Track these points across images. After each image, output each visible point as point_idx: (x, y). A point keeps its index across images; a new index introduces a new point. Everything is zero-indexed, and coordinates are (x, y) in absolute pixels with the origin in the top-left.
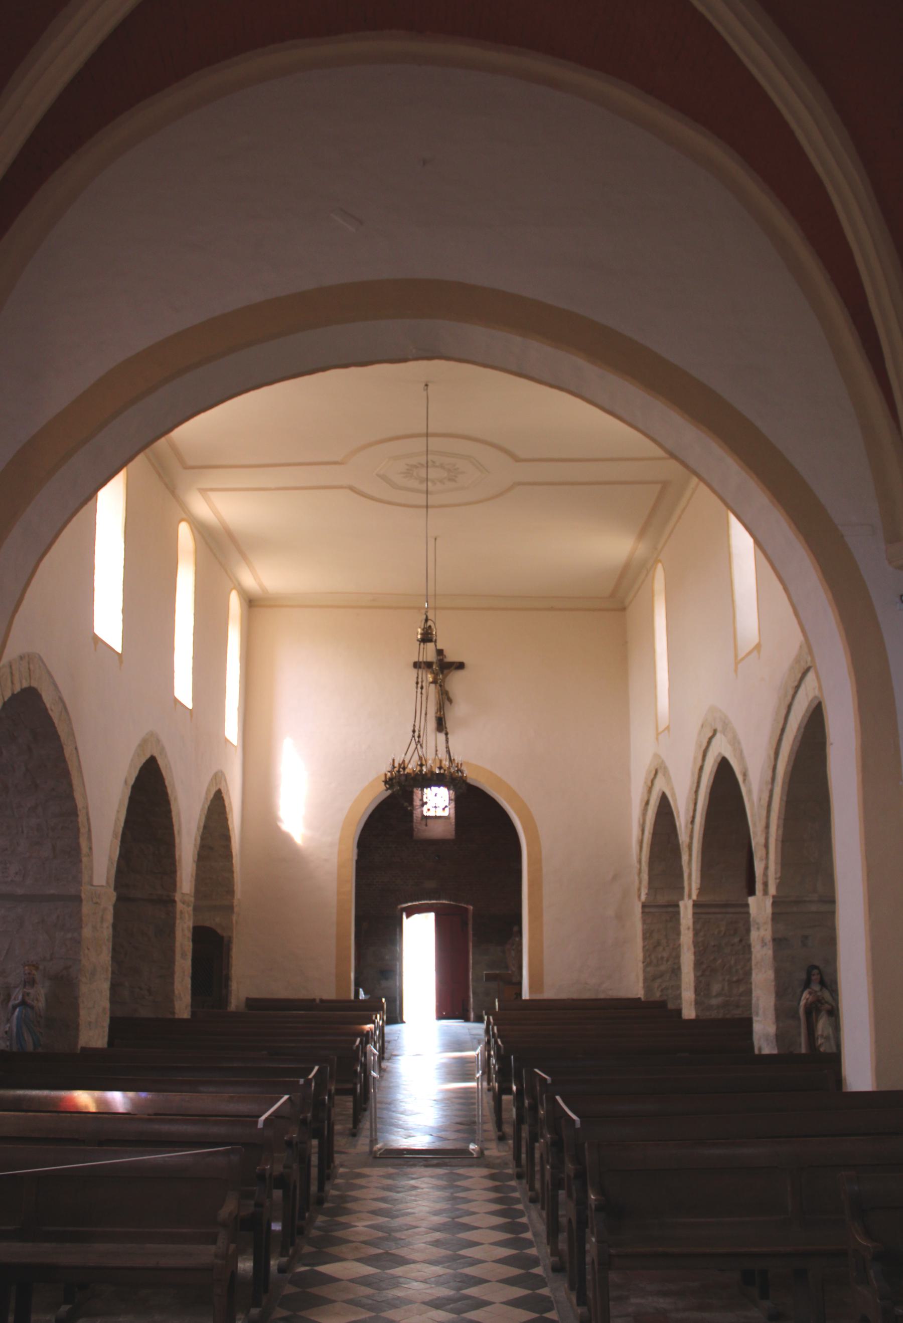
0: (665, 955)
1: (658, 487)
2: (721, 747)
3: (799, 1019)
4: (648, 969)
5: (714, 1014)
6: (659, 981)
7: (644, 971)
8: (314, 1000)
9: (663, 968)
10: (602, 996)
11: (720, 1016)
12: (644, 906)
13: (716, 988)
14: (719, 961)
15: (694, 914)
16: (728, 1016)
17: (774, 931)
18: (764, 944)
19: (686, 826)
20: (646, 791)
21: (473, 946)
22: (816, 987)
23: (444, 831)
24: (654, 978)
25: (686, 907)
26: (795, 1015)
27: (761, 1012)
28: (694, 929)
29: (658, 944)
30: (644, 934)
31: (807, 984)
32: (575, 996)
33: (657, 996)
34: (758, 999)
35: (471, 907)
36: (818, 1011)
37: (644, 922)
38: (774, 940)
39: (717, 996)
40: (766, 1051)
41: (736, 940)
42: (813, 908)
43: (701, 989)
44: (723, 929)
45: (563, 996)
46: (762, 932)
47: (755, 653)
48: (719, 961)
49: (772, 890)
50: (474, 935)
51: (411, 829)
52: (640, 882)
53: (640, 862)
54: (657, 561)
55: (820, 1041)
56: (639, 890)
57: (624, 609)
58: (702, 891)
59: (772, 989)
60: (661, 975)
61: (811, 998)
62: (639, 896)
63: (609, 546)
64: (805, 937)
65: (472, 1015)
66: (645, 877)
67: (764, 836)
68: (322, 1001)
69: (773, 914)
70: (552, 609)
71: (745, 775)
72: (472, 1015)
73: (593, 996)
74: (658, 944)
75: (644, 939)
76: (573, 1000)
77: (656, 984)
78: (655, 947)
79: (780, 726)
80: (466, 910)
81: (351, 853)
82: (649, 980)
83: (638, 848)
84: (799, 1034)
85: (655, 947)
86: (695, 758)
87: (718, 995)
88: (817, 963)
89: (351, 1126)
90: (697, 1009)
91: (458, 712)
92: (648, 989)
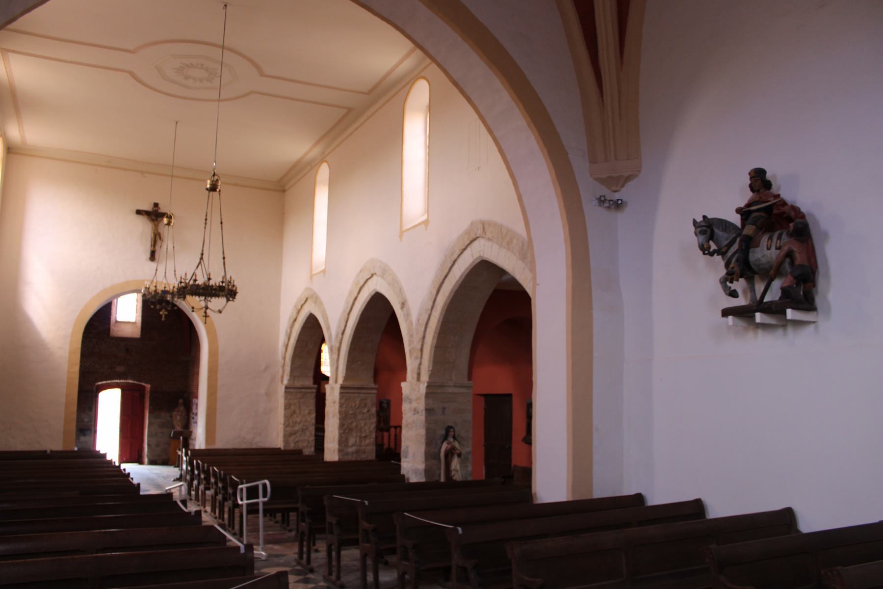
0: (298, 420)
1: (345, 111)
2: (378, 285)
3: (440, 460)
4: (288, 429)
5: (349, 458)
6: (294, 436)
7: (285, 430)
8: (45, 451)
9: (296, 428)
10: (254, 447)
11: (354, 459)
12: (286, 388)
13: (352, 441)
14: (354, 424)
15: (341, 393)
16: (359, 459)
17: (427, 404)
18: (416, 411)
19: (337, 336)
20: (295, 312)
21: (150, 413)
22: (451, 439)
23: (135, 332)
24: (291, 435)
25: (332, 389)
26: (437, 457)
27: (410, 456)
28: (340, 403)
29: (294, 412)
30: (285, 406)
31: (445, 438)
32: (237, 446)
33: (292, 446)
34: (407, 447)
35: (148, 386)
36: (453, 454)
37: (286, 398)
38: (426, 410)
39: (352, 446)
40: (414, 479)
41: (365, 410)
42: (450, 390)
43: (343, 442)
44: (358, 403)
45: (229, 446)
46: (414, 405)
47: (423, 226)
48: (354, 424)
49: (425, 377)
50: (150, 405)
51: (109, 329)
52: (283, 372)
53: (284, 358)
54: (322, 161)
55: (453, 473)
56: (282, 377)
57: (284, 191)
58: (346, 378)
59: (423, 440)
60: (295, 433)
61: (449, 446)
62: (282, 381)
63: (291, 147)
64: (444, 408)
65: (146, 460)
66: (288, 369)
67: (420, 343)
68: (51, 451)
69: (427, 393)
70: (236, 185)
71: (403, 305)
72: (146, 460)
73: (249, 447)
74: (294, 412)
75: (285, 409)
76: (236, 449)
77: (291, 439)
78: (292, 415)
79: (444, 274)
80: (144, 387)
81: (79, 345)
82: (287, 436)
83: (284, 350)
84: (439, 469)
85: (292, 415)
86: (351, 292)
87: (352, 446)
88: (450, 424)
89: (296, 556)
90: (339, 455)
91: (167, 245)
92: (286, 441)
